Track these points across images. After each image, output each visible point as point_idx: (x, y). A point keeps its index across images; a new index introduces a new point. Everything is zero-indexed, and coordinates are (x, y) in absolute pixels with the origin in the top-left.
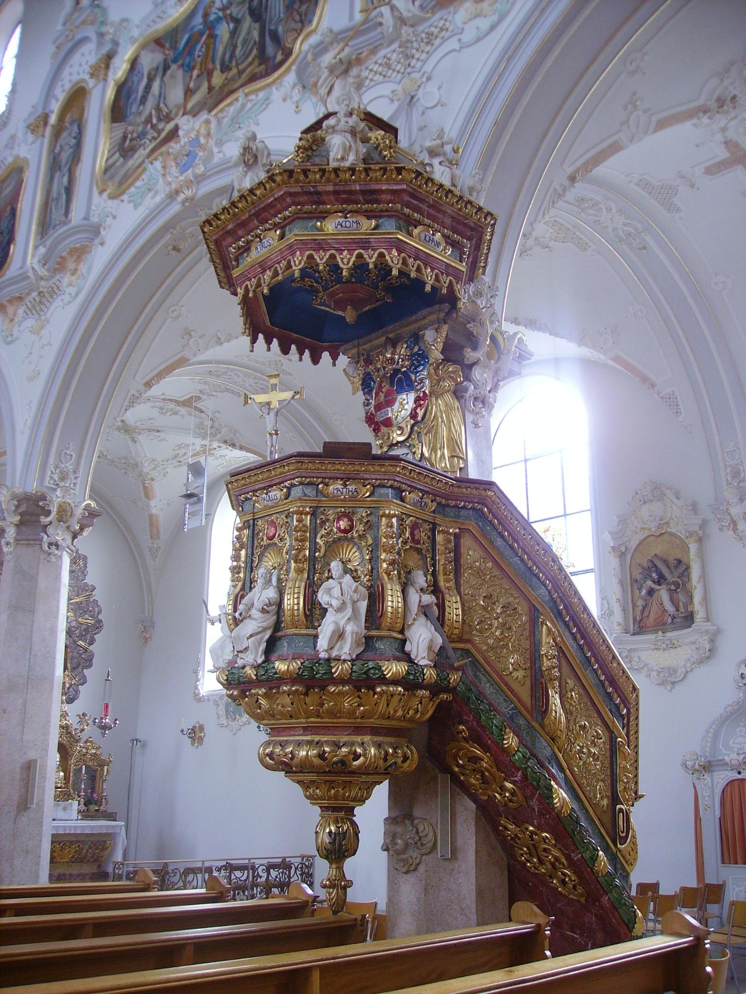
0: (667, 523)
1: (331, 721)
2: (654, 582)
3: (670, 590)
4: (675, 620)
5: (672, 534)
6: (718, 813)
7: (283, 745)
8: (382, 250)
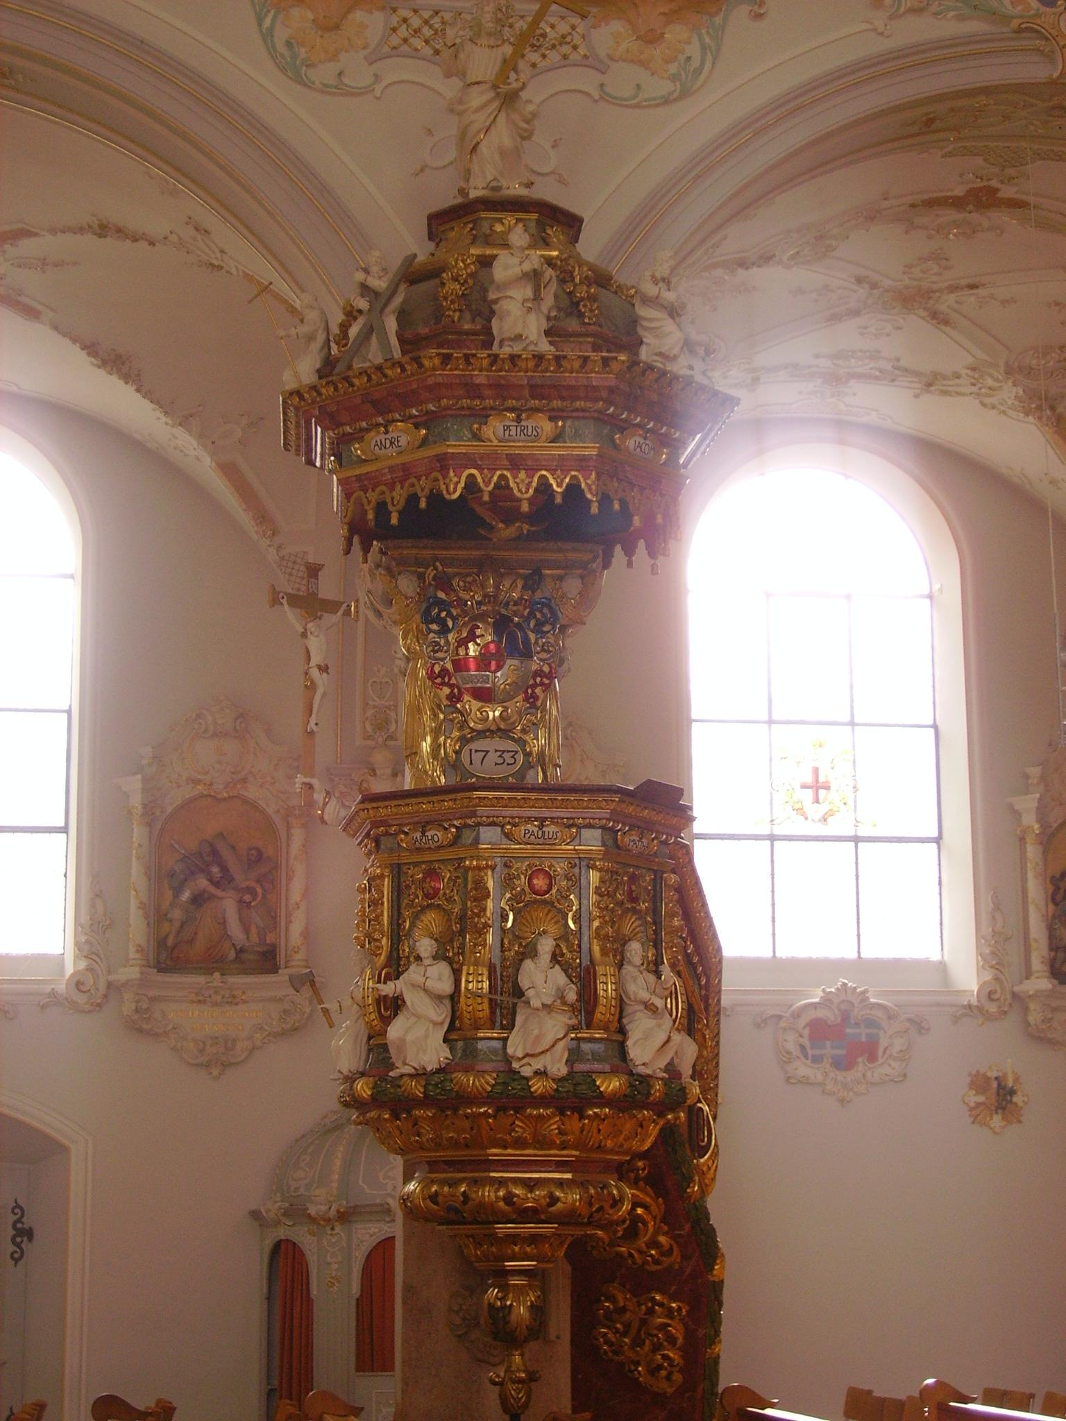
0: (244, 780)
1: (517, 1152)
2: (211, 881)
3: (240, 901)
4: (245, 956)
5: (245, 801)
6: (356, 1289)
7: (453, 1184)
8: (544, 473)
